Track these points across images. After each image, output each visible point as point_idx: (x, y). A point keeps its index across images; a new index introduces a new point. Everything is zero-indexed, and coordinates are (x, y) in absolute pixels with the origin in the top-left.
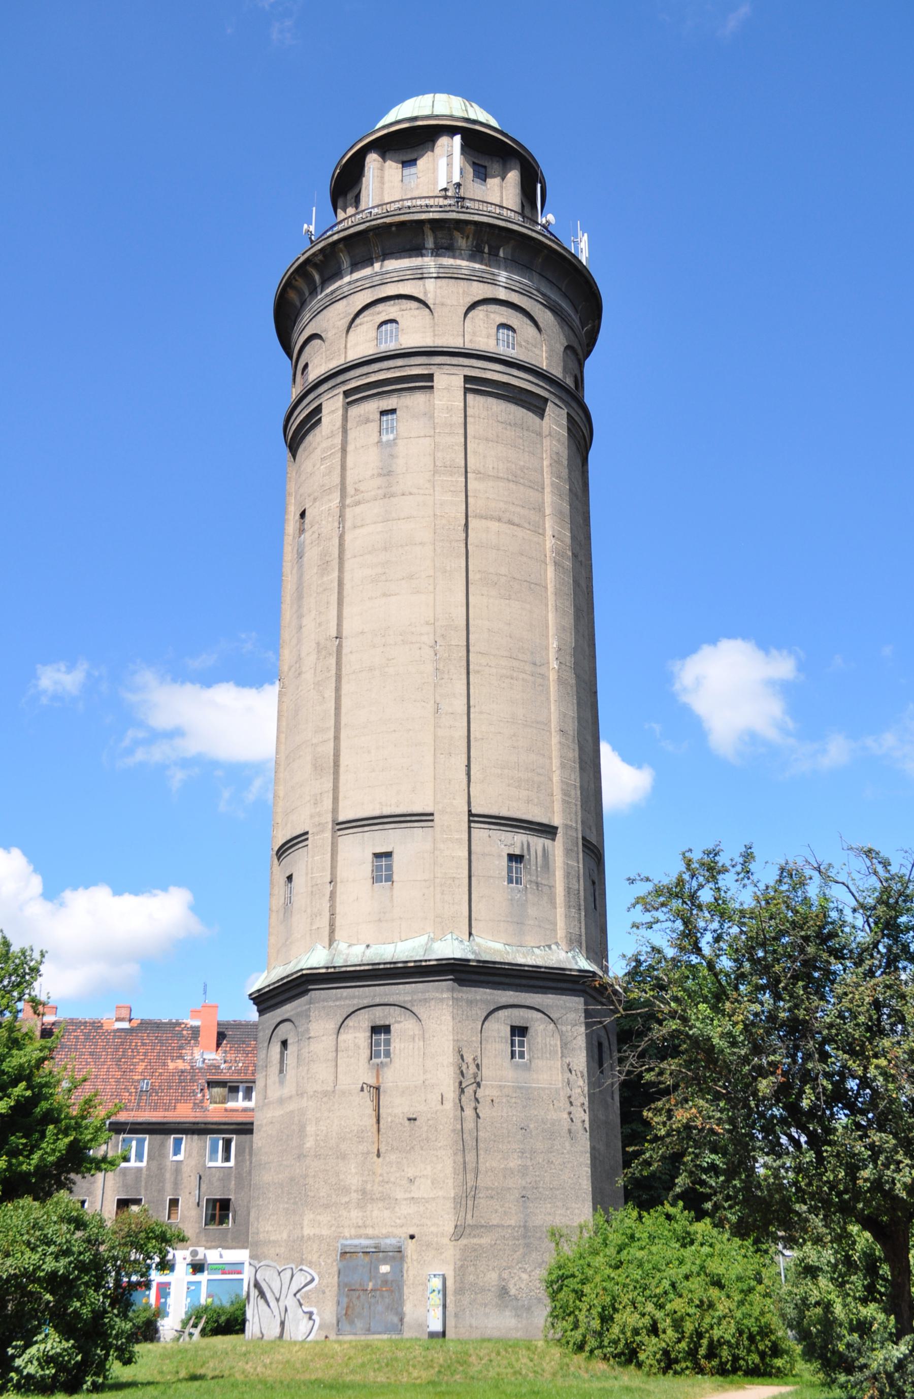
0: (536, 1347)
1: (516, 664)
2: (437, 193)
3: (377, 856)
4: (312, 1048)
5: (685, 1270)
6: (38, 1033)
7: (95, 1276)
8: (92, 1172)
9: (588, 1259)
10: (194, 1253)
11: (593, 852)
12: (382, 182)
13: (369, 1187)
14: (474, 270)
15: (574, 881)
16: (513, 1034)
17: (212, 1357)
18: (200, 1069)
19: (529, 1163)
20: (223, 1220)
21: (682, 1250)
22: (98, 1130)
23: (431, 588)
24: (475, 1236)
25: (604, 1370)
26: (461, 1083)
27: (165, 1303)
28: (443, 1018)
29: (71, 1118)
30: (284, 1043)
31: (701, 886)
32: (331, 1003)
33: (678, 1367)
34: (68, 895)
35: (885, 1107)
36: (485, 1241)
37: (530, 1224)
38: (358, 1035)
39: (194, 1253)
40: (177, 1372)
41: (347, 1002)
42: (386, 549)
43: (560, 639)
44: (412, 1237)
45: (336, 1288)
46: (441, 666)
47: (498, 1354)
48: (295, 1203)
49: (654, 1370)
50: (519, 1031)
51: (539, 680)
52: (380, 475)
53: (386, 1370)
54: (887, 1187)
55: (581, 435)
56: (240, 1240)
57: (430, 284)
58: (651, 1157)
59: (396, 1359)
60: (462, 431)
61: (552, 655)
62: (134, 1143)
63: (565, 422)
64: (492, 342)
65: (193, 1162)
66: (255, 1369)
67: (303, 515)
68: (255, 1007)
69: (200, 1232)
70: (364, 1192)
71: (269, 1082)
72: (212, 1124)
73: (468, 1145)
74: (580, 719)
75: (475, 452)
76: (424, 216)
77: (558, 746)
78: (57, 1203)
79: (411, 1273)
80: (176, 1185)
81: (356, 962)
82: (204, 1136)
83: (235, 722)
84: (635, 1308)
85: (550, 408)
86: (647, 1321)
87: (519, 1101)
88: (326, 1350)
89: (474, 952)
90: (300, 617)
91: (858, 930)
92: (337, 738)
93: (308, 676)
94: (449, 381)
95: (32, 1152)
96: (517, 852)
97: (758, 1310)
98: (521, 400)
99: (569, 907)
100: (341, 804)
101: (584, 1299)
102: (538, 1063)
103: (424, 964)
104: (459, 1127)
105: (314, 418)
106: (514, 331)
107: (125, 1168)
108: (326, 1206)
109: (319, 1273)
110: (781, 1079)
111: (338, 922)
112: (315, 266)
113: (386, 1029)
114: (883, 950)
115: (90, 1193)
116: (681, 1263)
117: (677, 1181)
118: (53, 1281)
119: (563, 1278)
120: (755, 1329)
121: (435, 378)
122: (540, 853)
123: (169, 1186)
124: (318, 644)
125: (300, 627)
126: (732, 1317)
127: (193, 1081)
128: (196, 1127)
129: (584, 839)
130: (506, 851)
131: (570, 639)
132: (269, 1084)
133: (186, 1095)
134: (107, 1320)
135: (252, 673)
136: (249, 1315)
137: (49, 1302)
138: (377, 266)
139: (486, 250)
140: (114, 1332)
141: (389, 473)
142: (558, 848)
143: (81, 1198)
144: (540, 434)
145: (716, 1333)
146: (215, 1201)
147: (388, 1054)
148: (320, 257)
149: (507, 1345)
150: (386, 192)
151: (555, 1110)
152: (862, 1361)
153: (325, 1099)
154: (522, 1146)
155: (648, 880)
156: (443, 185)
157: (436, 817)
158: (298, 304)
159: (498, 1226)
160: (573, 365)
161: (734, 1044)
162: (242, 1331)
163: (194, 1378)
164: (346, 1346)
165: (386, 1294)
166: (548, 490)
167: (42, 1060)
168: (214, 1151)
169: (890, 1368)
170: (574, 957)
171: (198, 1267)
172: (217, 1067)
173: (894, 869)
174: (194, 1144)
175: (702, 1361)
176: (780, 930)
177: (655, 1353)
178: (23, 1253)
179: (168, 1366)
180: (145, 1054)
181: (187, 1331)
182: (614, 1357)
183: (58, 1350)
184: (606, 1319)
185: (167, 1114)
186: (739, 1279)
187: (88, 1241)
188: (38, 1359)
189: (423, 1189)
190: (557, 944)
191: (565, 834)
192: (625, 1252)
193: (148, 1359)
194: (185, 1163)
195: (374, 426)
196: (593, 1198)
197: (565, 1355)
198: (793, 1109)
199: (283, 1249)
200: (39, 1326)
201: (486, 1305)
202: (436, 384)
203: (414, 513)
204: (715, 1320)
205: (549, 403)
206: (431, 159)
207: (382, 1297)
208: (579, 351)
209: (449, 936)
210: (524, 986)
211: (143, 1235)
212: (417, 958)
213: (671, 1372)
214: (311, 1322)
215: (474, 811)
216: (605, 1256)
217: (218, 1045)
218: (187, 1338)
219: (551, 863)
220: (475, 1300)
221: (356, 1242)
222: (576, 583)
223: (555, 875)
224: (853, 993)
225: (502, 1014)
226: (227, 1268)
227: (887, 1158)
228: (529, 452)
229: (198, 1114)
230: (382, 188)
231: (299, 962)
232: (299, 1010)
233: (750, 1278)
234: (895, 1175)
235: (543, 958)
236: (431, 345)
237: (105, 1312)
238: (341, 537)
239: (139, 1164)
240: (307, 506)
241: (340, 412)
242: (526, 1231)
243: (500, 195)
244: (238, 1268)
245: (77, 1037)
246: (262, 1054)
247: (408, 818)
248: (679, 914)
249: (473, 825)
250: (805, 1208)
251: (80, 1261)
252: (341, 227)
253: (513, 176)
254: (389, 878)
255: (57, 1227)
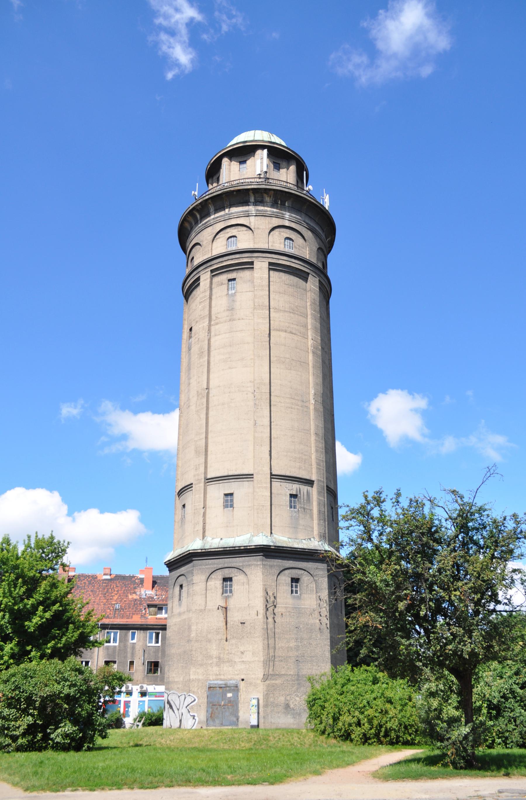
0: (302, 732)
1: (294, 401)
2: (256, 176)
3: (226, 495)
4: (194, 589)
5: (374, 695)
6: (66, 581)
7: (88, 697)
8: (91, 647)
9: (328, 691)
10: (142, 687)
11: (332, 493)
12: (230, 171)
13: (222, 656)
14: (273, 212)
15: (322, 507)
16: (292, 582)
17: (146, 736)
18: (144, 598)
19: (300, 644)
20: (155, 671)
21: (373, 686)
22: (93, 627)
23: (252, 365)
24: (273, 680)
25: (334, 743)
26: (266, 606)
27: (128, 710)
28: (258, 574)
29: (81, 622)
30: (181, 586)
31: (372, 509)
32: (204, 567)
33: (370, 741)
34: (76, 514)
35: (459, 615)
36: (278, 682)
37: (300, 674)
38: (216, 582)
39: (142, 687)
40: (129, 743)
41: (211, 566)
42: (230, 346)
43: (315, 389)
44: (243, 680)
45: (206, 704)
46: (257, 402)
47: (283, 735)
48: (186, 663)
49: (359, 743)
50: (295, 580)
51: (305, 409)
52: (228, 310)
53: (229, 743)
54: (459, 653)
55: (326, 291)
56: (161, 681)
57: (252, 219)
58: (349, 640)
59: (234, 738)
60: (267, 289)
61: (311, 397)
62: (112, 634)
63: (318, 284)
64: (282, 246)
65: (141, 644)
66: (166, 742)
67: (191, 329)
68: (167, 569)
69: (144, 677)
70: (219, 658)
71: (174, 605)
72: (150, 625)
73: (270, 635)
74: (325, 428)
75: (274, 299)
76: (249, 187)
77: (314, 441)
78: (69, 662)
79: (243, 697)
80: (133, 654)
81: (216, 546)
82: (146, 631)
83: (156, 431)
84: (350, 713)
85: (310, 277)
86: (355, 720)
87: (295, 614)
88: (200, 734)
89: (273, 542)
90: (189, 379)
91: (449, 529)
92: (207, 438)
93: (193, 408)
94: (261, 265)
95: (61, 637)
96: (294, 493)
97: (409, 714)
98: (296, 274)
99: (320, 520)
100: (209, 470)
101: (325, 709)
102: (304, 596)
103: (248, 547)
104: (266, 627)
105: (196, 283)
106: (293, 241)
107: (108, 646)
108: (201, 665)
109: (198, 697)
110: (409, 602)
111: (207, 528)
112: (198, 211)
113: (230, 579)
114: (461, 539)
115: (92, 658)
116: (372, 692)
117: (361, 651)
118: (68, 698)
119: (315, 700)
120: (407, 723)
121: (255, 263)
122: (305, 494)
123: (129, 655)
124: (198, 392)
125: (189, 384)
126: (396, 717)
127: (141, 604)
128: (142, 626)
129: (327, 486)
130: (289, 492)
131: (320, 389)
132: (173, 605)
133: (137, 611)
134: (94, 718)
135: (162, 407)
136: (165, 717)
137: (66, 708)
138: (227, 210)
139: (279, 203)
140: (98, 723)
141: (232, 309)
142: (314, 491)
143: (87, 660)
144: (305, 290)
145: (389, 725)
146: (151, 662)
147: (231, 591)
148: (200, 207)
149: (288, 731)
150: (232, 176)
151: (313, 619)
152: (448, 736)
153: (201, 613)
154: (296, 636)
155: (348, 506)
156: (258, 172)
157: (255, 476)
158: (189, 229)
159: (284, 675)
160: (322, 257)
161: (387, 585)
162: (162, 724)
163: (137, 745)
164: (210, 732)
165: (230, 707)
166: (309, 317)
167: (67, 593)
168: (151, 638)
169: (461, 739)
170: (322, 544)
171: (143, 694)
172: (152, 598)
173: (466, 500)
174: (141, 635)
175: (382, 739)
176: (410, 530)
177: (359, 735)
178: (53, 685)
179: (125, 740)
180: (118, 591)
181: (135, 724)
182: (339, 737)
183: (71, 731)
184: (336, 719)
185: (128, 620)
186: (400, 699)
187: (85, 680)
188: (61, 735)
189: (248, 657)
190: (314, 538)
191: (318, 484)
192: (345, 687)
193: (114, 736)
194: (137, 644)
195: (225, 287)
196: (331, 661)
197: (316, 736)
198: (417, 616)
199: (181, 685)
200: (61, 720)
201: (279, 713)
202: (255, 266)
203: (245, 329)
204: (388, 719)
205: (310, 275)
206: (253, 160)
207: (228, 708)
208: (325, 250)
209: (261, 534)
210: (298, 558)
211: (111, 677)
212: (245, 545)
213: (367, 744)
214: (194, 720)
215: (273, 473)
216: (335, 689)
217: (153, 587)
218: (136, 727)
219: (311, 498)
220: (273, 710)
221: (216, 682)
222: (323, 362)
223: (313, 504)
224: (444, 560)
225: (287, 572)
226: (158, 694)
227: (460, 639)
228: (300, 299)
229: (143, 621)
230: (230, 174)
231: (188, 546)
232: (188, 570)
233: (405, 699)
234: (463, 647)
235: (307, 544)
236: (253, 247)
237: (93, 714)
238: (209, 340)
239: (115, 644)
240: (193, 325)
241: (209, 280)
242: (298, 677)
243: (287, 177)
244: (161, 694)
245: (85, 583)
246: (170, 592)
247: (241, 477)
248: (361, 522)
249: (272, 480)
250: (421, 664)
251: (81, 690)
252: (210, 192)
253: (293, 168)
254: (232, 506)
255: (70, 673)
